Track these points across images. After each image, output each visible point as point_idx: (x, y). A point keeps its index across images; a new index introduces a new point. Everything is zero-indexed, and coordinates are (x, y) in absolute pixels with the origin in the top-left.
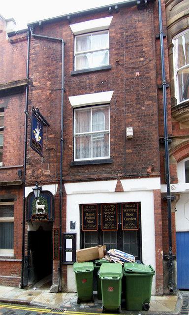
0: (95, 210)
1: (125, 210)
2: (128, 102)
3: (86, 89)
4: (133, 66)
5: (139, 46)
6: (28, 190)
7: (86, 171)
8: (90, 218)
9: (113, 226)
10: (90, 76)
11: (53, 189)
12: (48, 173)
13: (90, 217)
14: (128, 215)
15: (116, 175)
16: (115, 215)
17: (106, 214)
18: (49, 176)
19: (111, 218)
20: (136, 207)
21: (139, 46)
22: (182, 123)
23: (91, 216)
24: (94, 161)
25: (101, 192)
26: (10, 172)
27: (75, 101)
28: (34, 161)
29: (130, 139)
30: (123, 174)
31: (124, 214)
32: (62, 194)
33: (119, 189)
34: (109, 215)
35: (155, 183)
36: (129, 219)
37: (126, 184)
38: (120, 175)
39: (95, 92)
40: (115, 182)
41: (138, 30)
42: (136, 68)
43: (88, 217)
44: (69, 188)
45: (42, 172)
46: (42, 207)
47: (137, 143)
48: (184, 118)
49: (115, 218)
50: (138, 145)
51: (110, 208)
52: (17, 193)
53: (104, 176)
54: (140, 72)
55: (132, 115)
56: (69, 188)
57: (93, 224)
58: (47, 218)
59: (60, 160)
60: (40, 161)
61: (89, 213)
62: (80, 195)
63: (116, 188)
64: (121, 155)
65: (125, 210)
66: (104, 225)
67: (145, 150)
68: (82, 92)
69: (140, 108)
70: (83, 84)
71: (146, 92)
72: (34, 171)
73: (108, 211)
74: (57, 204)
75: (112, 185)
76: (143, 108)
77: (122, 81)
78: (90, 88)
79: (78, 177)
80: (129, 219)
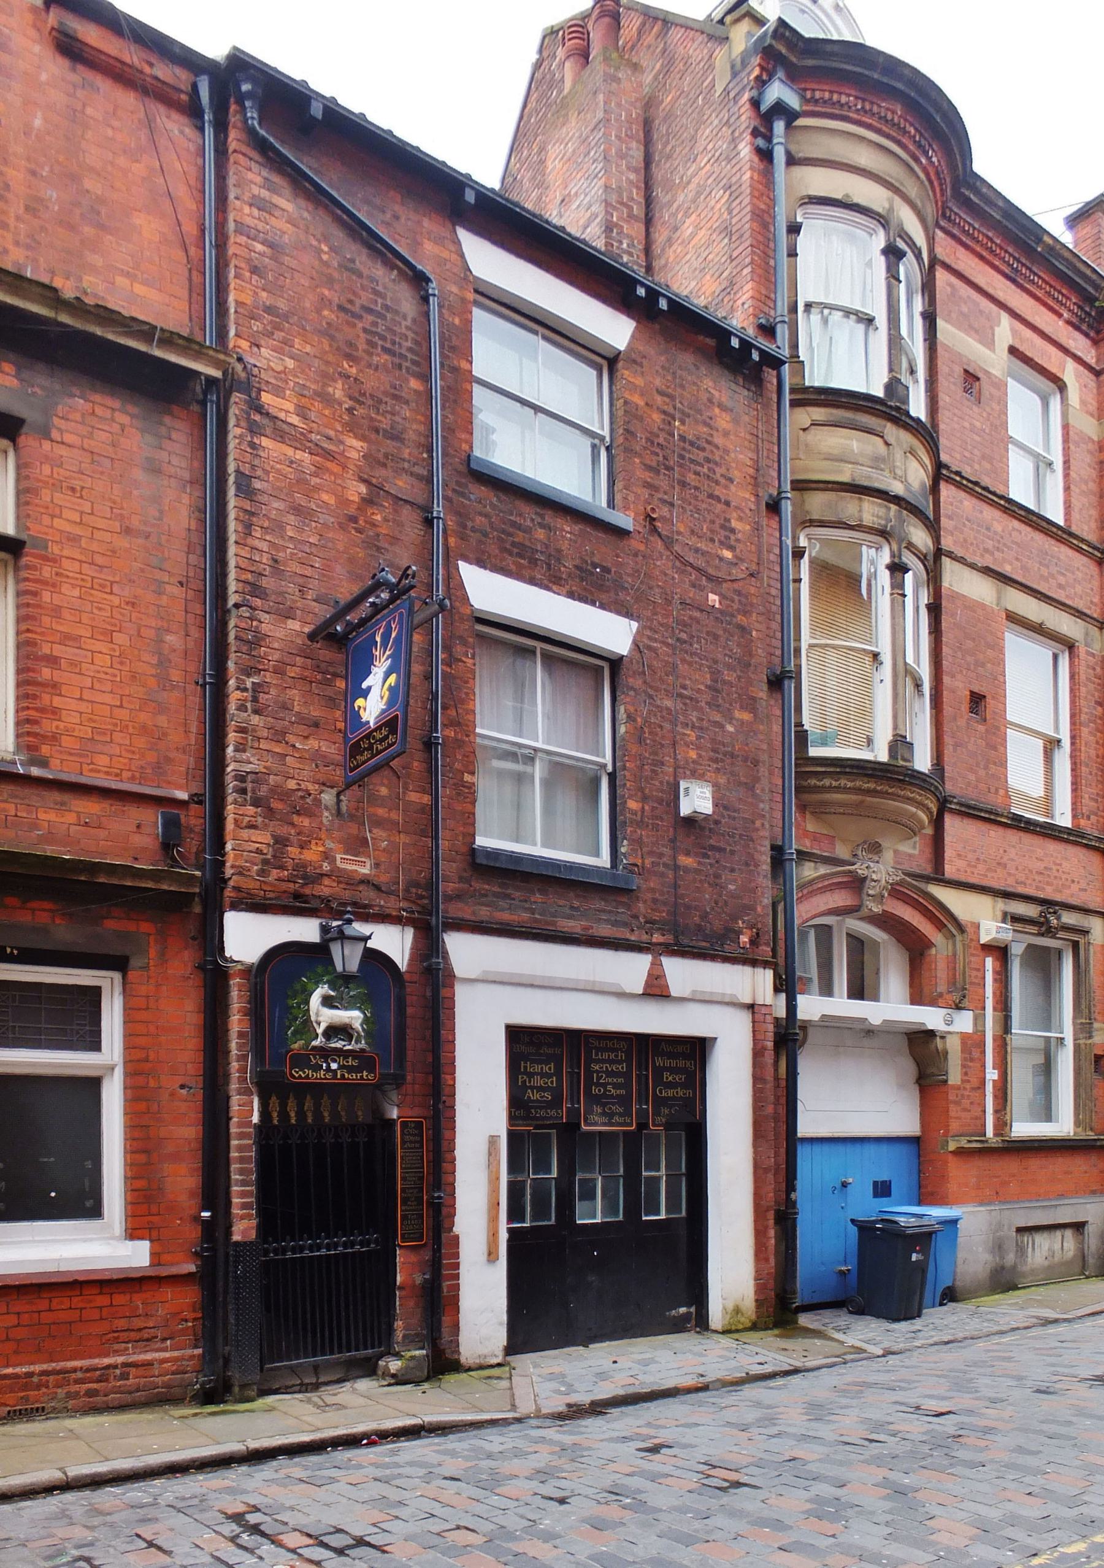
0: (558, 1051)
1: (659, 1062)
2: (684, 687)
3: (534, 562)
4: (700, 563)
5: (718, 500)
6: (247, 937)
7: (538, 897)
8: (538, 1081)
9: (621, 1115)
10: (549, 517)
11: (394, 942)
12: (365, 870)
13: (541, 1079)
14: (668, 1077)
15: (645, 937)
16: (627, 1075)
17: (597, 1072)
18: (365, 881)
19: (616, 1086)
20: (695, 1051)
21: (718, 500)
22: (812, 813)
23: (543, 1075)
24: (571, 867)
25: (593, 989)
26: (90, 807)
27: (489, 591)
28: (284, 795)
29: (691, 822)
30: (669, 938)
31: (658, 1072)
32: (434, 975)
33: (656, 990)
34: (611, 1074)
35: (758, 984)
36: (670, 1093)
37: (680, 973)
38: (657, 938)
39: (571, 595)
40: (641, 963)
41: (718, 440)
42: (710, 578)
43: (531, 1075)
44: (464, 951)
45: (327, 856)
46: (353, 1017)
47: (712, 842)
48: (824, 803)
49: (627, 1085)
50: (713, 848)
51: (613, 1050)
52: (145, 927)
53: (604, 930)
54: (723, 597)
55: (699, 738)
56: (464, 951)
57: (549, 1105)
58: (371, 1070)
59: (428, 823)
60: (318, 802)
61: (533, 1062)
62: (505, 987)
63: (648, 984)
64: (662, 869)
65: (659, 1062)
66: (656, 1113)
67: (732, 870)
68: (520, 567)
69: (722, 727)
70: (520, 537)
71: (739, 677)
72: (281, 842)
73: (603, 1061)
74: (414, 1010)
75: (631, 969)
76: (730, 728)
77: (668, 602)
78: (549, 565)
79: (506, 916)
80: (670, 1093)
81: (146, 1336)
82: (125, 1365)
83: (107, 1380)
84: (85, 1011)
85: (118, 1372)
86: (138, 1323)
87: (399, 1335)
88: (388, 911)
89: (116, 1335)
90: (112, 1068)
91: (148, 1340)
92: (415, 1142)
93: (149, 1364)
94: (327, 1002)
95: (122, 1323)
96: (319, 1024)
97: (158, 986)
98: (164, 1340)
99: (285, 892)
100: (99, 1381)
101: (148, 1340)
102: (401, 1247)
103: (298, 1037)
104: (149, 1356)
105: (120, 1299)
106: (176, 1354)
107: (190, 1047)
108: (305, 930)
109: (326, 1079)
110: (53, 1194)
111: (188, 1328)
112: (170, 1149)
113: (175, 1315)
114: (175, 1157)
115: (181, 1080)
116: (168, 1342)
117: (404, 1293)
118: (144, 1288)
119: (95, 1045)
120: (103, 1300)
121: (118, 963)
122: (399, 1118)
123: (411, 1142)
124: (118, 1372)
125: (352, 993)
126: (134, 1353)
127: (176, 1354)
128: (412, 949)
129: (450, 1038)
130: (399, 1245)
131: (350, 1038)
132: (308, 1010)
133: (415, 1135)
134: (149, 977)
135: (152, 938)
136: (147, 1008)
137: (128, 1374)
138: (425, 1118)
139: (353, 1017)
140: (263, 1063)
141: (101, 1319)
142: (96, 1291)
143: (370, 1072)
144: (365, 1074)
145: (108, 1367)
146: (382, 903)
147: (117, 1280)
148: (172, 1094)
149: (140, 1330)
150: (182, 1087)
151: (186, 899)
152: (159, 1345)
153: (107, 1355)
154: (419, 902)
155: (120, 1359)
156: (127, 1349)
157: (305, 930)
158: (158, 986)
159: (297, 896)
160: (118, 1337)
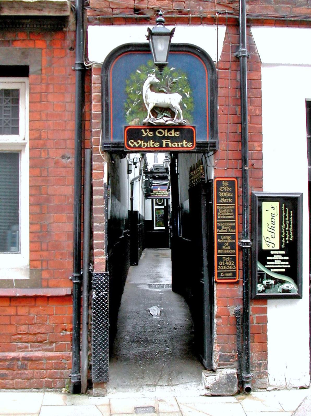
11: (210, 39)
32: (243, 64)
44: (265, 39)
56: (265, 39)
58: (191, 139)
81: (39, 339)
82: (24, 359)
83: (12, 369)
84: (9, 107)
85: (20, 363)
86: (34, 329)
87: (216, 357)
88: (204, 15)
89: (20, 336)
90: (24, 145)
91: (41, 342)
92: (229, 197)
93: (38, 359)
94: (153, 87)
95: (23, 328)
96: (148, 105)
97: (48, 85)
98: (51, 343)
99: (127, 8)
100: (8, 369)
101: (41, 342)
102: (217, 283)
103: (134, 115)
104: (40, 354)
105: (23, 311)
106: (58, 354)
107: (68, 128)
108: (137, 34)
109: (154, 147)
110: (139, 249)
111: (66, 335)
112: (54, 203)
113: (57, 325)
114: (59, 209)
115: (61, 152)
116: (54, 344)
117: (220, 321)
118: (49, 304)
119: (15, 131)
120: (11, 311)
121: (21, 71)
122: (215, 178)
123: (225, 198)
124: (20, 363)
125: (174, 80)
126: (31, 351)
127: (58, 354)
128: (224, 42)
129: (258, 112)
130: (216, 282)
131: (173, 114)
132: (141, 95)
133: (229, 192)
134: (42, 80)
135: (44, 50)
136: (40, 102)
137: (26, 365)
138: (236, 178)
139: (173, 99)
140: (107, 138)
141: (11, 324)
142: (7, 304)
143: (188, 141)
144: (185, 142)
145: (14, 359)
146: (201, 9)
147: (19, 297)
148: (57, 163)
149: (35, 334)
150: (63, 157)
151: (63, 20)
152: (47, 347)
153: (14, 351)
154: (230, 5)
155: (22, 354)
156: (27, 347)
157: (137, 34)
158: (48, 85)
159: (136, 10)
160: (20, 339)
